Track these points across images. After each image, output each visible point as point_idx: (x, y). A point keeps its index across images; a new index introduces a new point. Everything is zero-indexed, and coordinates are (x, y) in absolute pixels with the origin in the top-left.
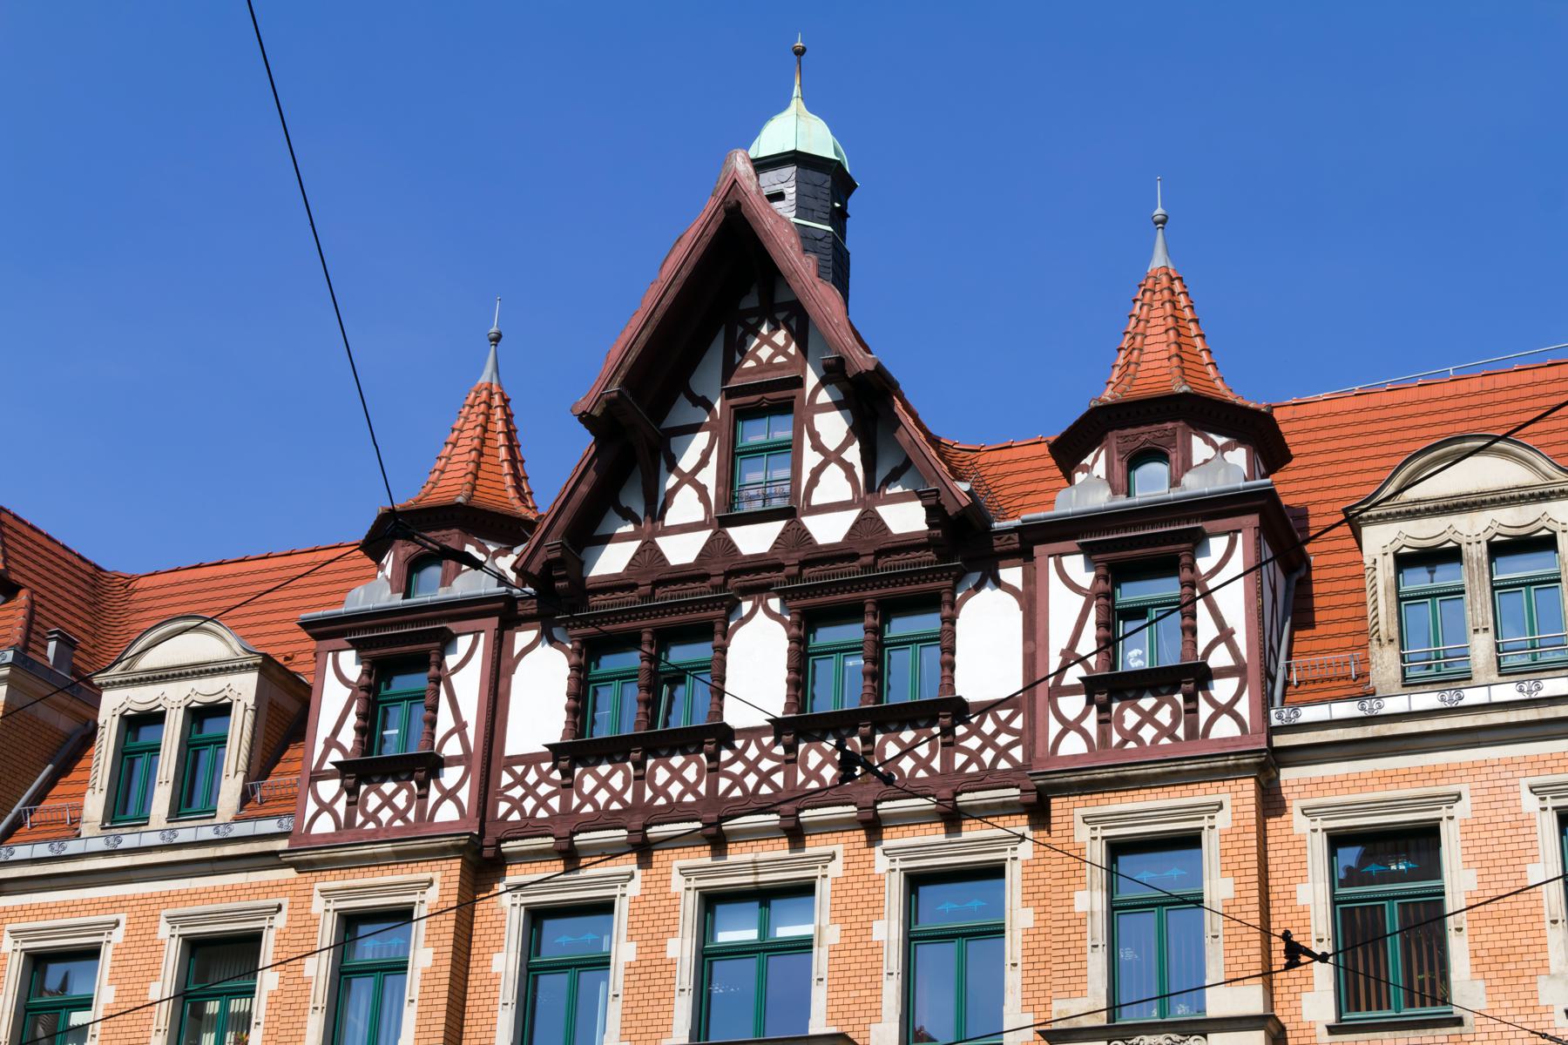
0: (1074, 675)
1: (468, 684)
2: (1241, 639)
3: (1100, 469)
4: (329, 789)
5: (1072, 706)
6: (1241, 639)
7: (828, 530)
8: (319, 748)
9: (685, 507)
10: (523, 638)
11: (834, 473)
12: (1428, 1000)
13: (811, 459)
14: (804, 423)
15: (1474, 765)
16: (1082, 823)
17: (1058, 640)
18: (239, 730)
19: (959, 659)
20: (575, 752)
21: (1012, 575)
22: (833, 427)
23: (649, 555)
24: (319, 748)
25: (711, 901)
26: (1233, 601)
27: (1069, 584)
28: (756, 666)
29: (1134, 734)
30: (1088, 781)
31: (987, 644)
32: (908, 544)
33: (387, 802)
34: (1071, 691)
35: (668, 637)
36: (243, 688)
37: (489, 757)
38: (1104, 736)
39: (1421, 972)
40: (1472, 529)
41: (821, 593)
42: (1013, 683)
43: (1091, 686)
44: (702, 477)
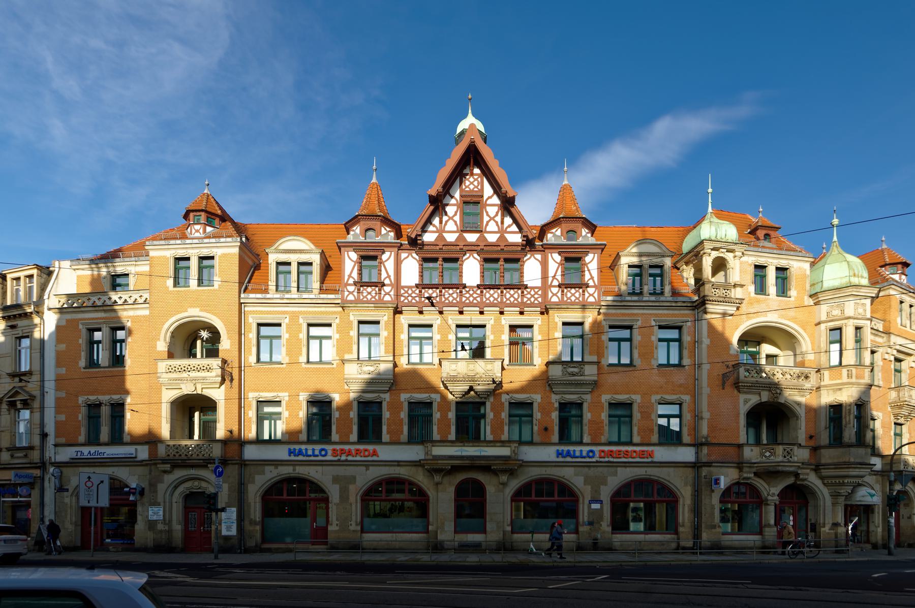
0: (556, 283)
1: (390, 265)
2: (392, 278)
3: (358, 231)
5: (555, 290)
6: (392, 278)
7: (492, 238)
8: (346, 278)
11: (492, 223)
15: (643, 314)
17: (551, 273)
18: (316, 269)
19: (464, 275)
21: (539, 256)
23: (441, 237)
24: (346, 278)
27: (555, 259)
28: (471, 270)
29: (366, 297)
30: (559, 306)
34: (555, 286)
36: (316, 259)
37: (397, 285)
38: (562, 298)
43: (355, 283)
44: (455, 218)
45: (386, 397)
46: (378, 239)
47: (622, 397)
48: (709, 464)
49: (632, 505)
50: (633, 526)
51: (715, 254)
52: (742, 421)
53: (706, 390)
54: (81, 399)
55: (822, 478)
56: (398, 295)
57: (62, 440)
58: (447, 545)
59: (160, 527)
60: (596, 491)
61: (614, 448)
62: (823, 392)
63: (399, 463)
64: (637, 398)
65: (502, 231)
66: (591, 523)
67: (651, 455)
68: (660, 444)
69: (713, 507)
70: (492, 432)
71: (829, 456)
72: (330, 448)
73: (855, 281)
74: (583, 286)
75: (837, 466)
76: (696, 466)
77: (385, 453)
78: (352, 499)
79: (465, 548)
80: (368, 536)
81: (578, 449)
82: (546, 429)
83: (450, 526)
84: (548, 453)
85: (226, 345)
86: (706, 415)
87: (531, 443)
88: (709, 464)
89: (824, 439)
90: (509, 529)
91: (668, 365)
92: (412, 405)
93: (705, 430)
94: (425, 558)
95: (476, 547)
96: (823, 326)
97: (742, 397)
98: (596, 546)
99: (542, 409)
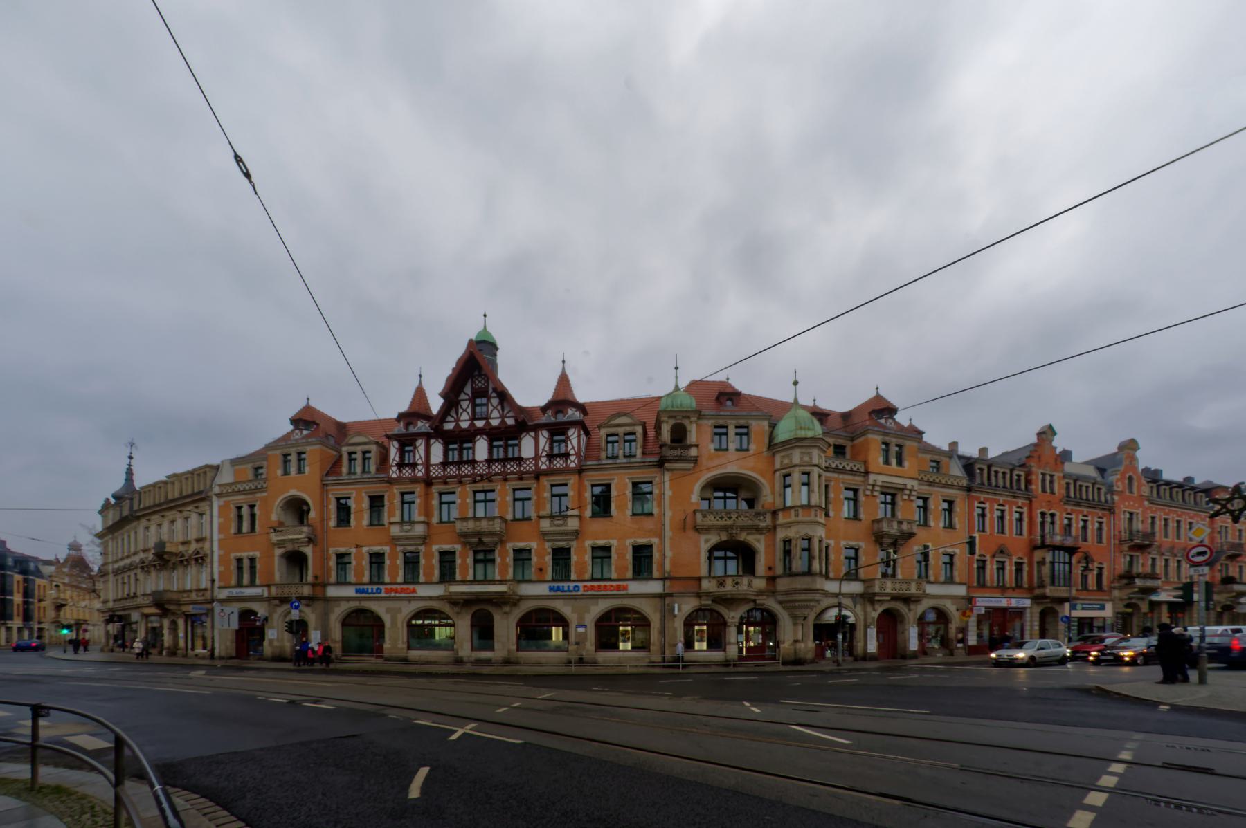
4: (394, 469)
5: (544, 459)
7: (495, 423)
9: (465, 416)
10: (432, 441)
12: (489, 557)
13: (491, 408)
14: (489, 398)
16: (545, 481)
17: (541, 447)
20: (445, 464)
21: (532, 434)
22: (495, 401)
23: (457, 426)
25: (475, 492)
26: (575, 442)
28: (481, 449)
30: (547, 473)
31: (527, 447)
32: (511, 427)
33: (407, 472)
35: (462, 442)
37: (427, 464)
40: (621, 430)
41: (493, 435)
42: (532, 455)
45: (422, 548)
46: (565, 419)
47: (601, 542)
48: (670, 595)
49: (621, 628)
50: (621, 646)
51: (672, 422)
52: (704, 556)
53: (668, 533)
54: (232, 555)
55: (781, 603)
56: (428, 471)
58: (465, 659)
59: (276, 644)
60: (581, 618)
61: (596, 584)
62: (779, 530)
63: (431, 598)
64: (614, 543)
65: (503, 417)
66: (577, 644)
67: (625, 588)
68: (634, 579)
69: (675, 630)
70: (500, 573)
71: (783, 584)
72: (382, 587)
74: (566, 456)
75: (787, 593)
76: (662, 596)
77: (422, 591)
78: (399, 625)
79: (479, 662)
80: (521, 654)
81: (566, 585)
82: (541, 570)
83: (467, 646)
84: (542, 589)
85: (312, 515)
86: (669, 554)
87: (529, 581)
88: (670, 595)
89: (779, 570)
90: (515, 647)
92: (371, 555)
93: (668, 567)
94: (574, 669)
95: (488, 662)
96: (778, 474)
97: (703, 538)
98: (581, 660)
99: (426, 555)
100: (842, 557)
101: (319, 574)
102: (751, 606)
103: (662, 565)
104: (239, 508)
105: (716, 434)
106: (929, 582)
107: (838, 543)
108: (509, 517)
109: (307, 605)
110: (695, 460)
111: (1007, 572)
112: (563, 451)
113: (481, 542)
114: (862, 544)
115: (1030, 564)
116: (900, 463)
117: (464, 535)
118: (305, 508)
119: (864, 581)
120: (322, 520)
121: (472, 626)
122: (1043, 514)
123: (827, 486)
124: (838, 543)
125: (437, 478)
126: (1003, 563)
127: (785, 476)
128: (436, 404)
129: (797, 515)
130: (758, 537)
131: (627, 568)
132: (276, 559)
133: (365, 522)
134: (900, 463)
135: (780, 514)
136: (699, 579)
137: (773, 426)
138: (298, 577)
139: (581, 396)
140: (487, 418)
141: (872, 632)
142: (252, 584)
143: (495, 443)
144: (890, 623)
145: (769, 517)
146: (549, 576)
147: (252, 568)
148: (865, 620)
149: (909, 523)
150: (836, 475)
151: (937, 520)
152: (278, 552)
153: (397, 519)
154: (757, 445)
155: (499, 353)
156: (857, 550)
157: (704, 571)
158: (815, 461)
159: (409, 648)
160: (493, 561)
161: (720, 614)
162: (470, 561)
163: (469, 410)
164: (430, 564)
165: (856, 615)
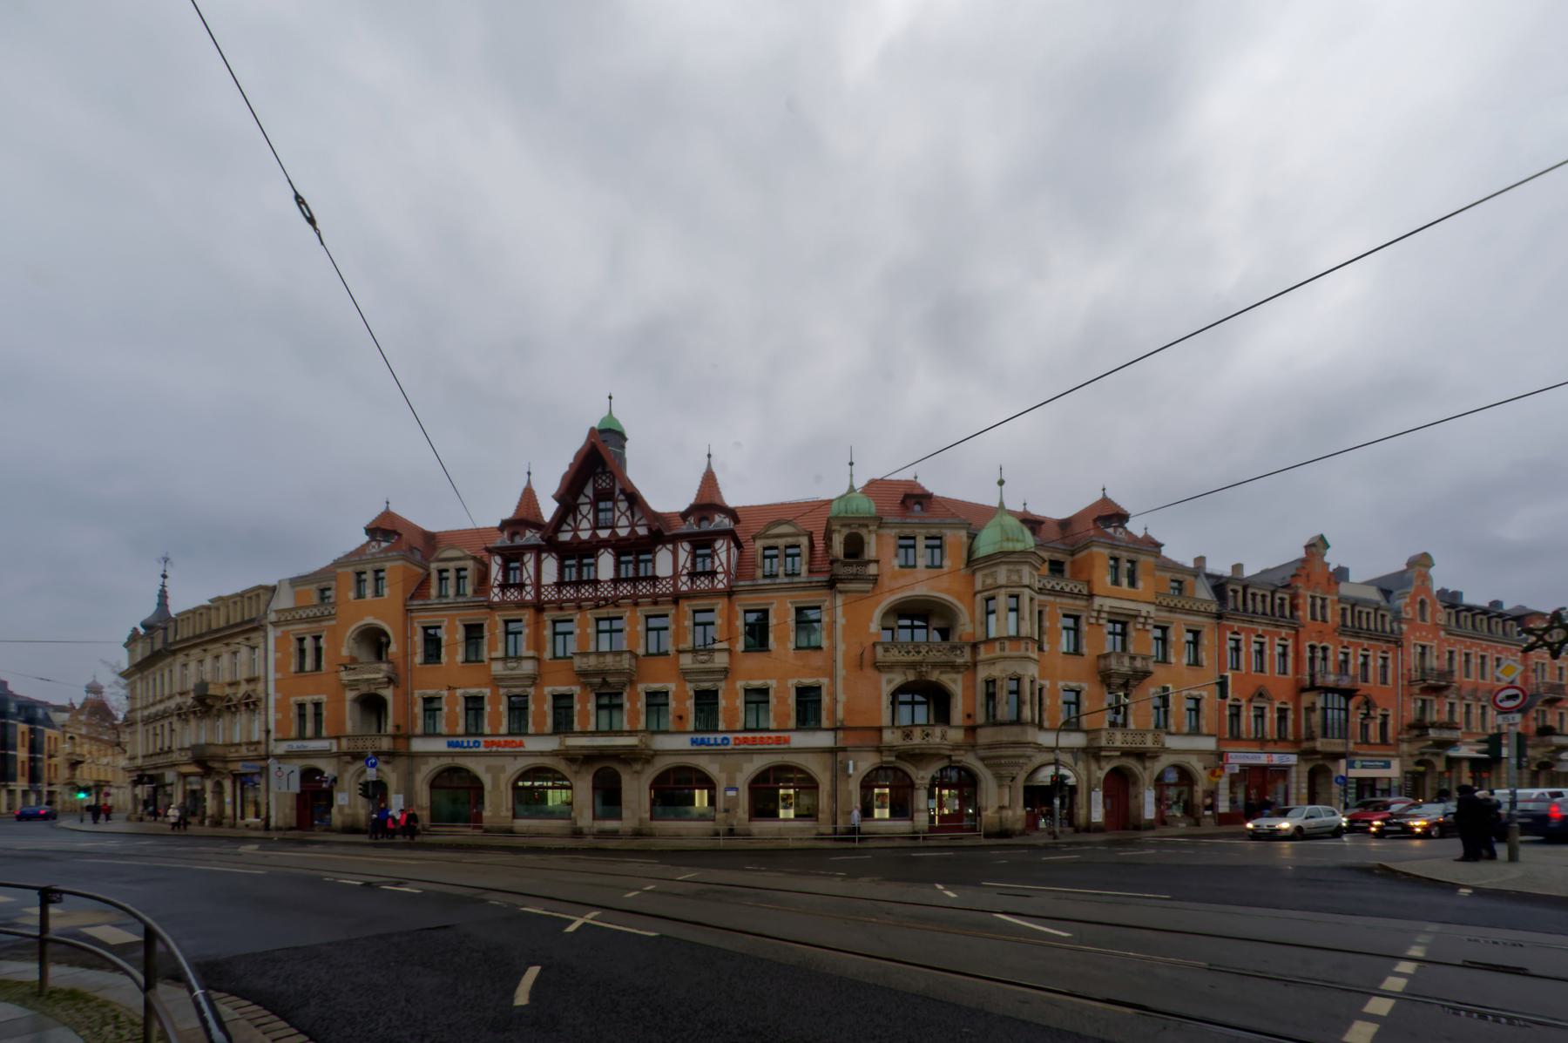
4: (496, 590)
5: (684, 579)
7: (623, 533)
9: (585, 524)
10: (544, 555)
13: (617, 514)
14: (615, 502)
16: (686, 606)
17: (681, 563)
20: (560, 584)
21: (670, 546)
22: (623, 506)
23: (576, 536)
25: (598, 620)
26: (723, 556)
28: (605, 566)
30: (689, 596)
31: (663, 563)
32: (643, 537)
33: (512, 595)
35: (582, 557)
37: (538, 584)
39: (487, 744)
40: (781, 542)
41: (621, 548)
42: (670, 573)
45: (531, 691)
46: (711, 527)
47: (756, 683)
48: (844, 749)
49: (781, 792)
50: (782, 813)
51: (846, 531)
52: (885, 701)
53: (841, 672)
54: (292, 700)
55: (982, 759)
56: (538, 593)
57: (280, 736)
58: (586, 830)
59: (347, 811)
60: (731, 778)
61: (750, 735)
62: (980, 668)
63: (542, 754)
64: (772, 683)
65: (632, 525)
66: (727, 811)
67: (787, 741)
68: (797, 729)
69: (850, 793)
70: (629, 722)
71: (985, 736)
72: (481, 740)
73: (1009, 546)
74: (713, 574)
75: (991, 747)
76: (833, 751)
77: (531, 744)
78: (503, 787)
79: (603, 834)
80: (656, 824)
81: (712, 736)
82: (680, 718)
83: (588, 813)
84: (682, 742)
85: (393, 648)
86: (841, 697)
87: (666, 732)
88: (844, 749)
89: (980, 718)
90: (648, 815)
91: (659, 654)
92: (467, 699)
93: (840, 714)
94: (722, 843)
95: (614, 834)
96: (979, 597)
97: (885, 677)
98: (731, 832)
99: (536, 699)
100: (1060, 702)
101: (401, 723)
102: (945, 763)
103: (833, 712)
104: (301, 640)
105: (901, 547)
106: (1169, 734)
107: (1054, 685)
108: (641, 651)
109: (387, 763)
110: (875, 580)
111: (1267, 720)
112: (708, 568)
113: (605, 683)
114: (1085, 685)
115: (1297, 711)
116: (1132, 583)
117: (583, 674)
118: (384, 640)
119: (1087, 732)
120: (405, 655)
121: (594, 788)
122: (1313, 648)
123: (1040, 613)
124: (1054, 685)
125: (550, 602)
126: (1263, 709)
127: (988, 600)
128: (548, 509)
129: (1003, 649)
130: (954, 676)
131: (788, 716)
132: (348, 705)
133: (460, 657)
134: (1132, 583)
135: (982, 648)
136: (880, 730)
137: (973, 537)
138: (375, 727)
139: (731, 499)
140: (613, 527)
141: (1098, 796)
142: (317, 735)
143: (623, 559)
144: (1120, 785)
145: (967, 651)
146: (691, 726)
147: (318, 715)
148: (1089, 781)
149: (1144, 658)
150: (1051, 599)
151: (1179, 655)
152: (350, 695)
153: (500, 653)
154: (952, 561)
155: (628, 445)
156: (1078, 693)
157: (886, 720)
158: (1026, 581)
159: (515, 816)
160: (620, 707)
161: (906, 774)
162: (591, 706)
163: (591, 516)
164: (541, 710)
165: (1077, 775)
